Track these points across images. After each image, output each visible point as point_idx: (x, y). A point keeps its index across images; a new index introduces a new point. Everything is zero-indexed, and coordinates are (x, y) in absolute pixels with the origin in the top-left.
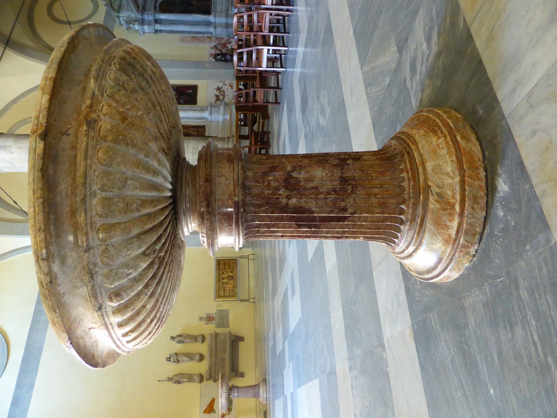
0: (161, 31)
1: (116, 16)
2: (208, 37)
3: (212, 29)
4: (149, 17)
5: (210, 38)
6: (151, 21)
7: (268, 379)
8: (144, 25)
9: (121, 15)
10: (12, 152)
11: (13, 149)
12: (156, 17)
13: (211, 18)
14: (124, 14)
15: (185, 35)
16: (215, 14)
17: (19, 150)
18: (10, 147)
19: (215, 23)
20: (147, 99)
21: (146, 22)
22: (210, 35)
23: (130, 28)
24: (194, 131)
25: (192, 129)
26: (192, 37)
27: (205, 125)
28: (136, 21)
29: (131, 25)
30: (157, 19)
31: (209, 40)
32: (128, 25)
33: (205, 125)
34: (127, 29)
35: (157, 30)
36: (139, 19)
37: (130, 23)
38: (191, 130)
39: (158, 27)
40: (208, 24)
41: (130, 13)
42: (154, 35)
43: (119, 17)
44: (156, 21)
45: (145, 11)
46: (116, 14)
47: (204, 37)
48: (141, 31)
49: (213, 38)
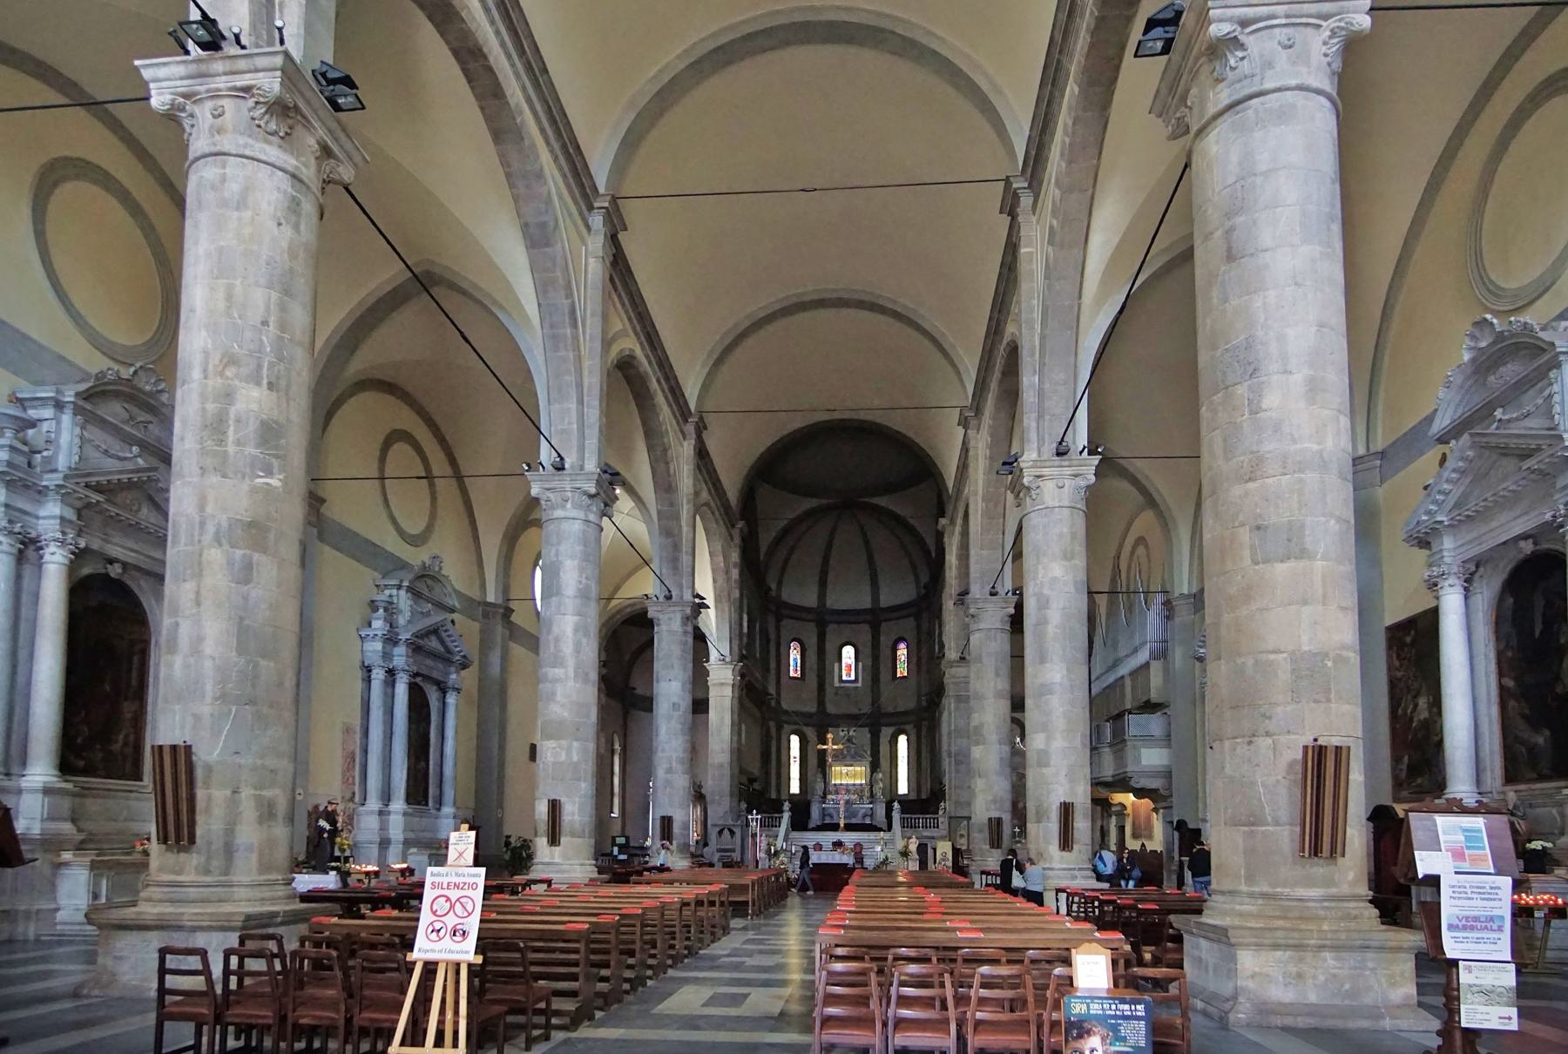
0: (368, 680)
1: (401, 581)
2: (354, 794)
3: (373, 804)
4: (400, 656)
5: (352, 799)
6: (391, 660)
7: (1308, 1014)
8: (384, 642)
9: (402, 593)
10: (280, 224)
11: (287, 231)
12: (52, 548)
13: (398, 805)
14: (403, 600)
15: (358, 736)
16: (411, 815)
17: (285, 244)
18: (296, 227)
19: (389, 813)
20: (1211, 972)
21: (388, 648)
22: (357, 799)
23: (375, 610)
24: (126, 744)
25: (132, 738)
26: (353, 753)
27: (141, 780)
28: (391, 626)
29: (381, 611)
30: (41, 548)
31: (348, 795)
32: (383, 604)
33: (141, 780)
34: (373, 601)
35: (370, 671)
36: (398, 634)
37: (386, 610)
38: (127, 736)
39: (378, 675)
40: (386, 798)
41: (408, 615)
42: (358, 664)
43: (399, 587)
44: (391, 673)
45: (414, 650)
46: (406, 584)
47: (354, 784)
48: (371, 634)
49: (351, 805)
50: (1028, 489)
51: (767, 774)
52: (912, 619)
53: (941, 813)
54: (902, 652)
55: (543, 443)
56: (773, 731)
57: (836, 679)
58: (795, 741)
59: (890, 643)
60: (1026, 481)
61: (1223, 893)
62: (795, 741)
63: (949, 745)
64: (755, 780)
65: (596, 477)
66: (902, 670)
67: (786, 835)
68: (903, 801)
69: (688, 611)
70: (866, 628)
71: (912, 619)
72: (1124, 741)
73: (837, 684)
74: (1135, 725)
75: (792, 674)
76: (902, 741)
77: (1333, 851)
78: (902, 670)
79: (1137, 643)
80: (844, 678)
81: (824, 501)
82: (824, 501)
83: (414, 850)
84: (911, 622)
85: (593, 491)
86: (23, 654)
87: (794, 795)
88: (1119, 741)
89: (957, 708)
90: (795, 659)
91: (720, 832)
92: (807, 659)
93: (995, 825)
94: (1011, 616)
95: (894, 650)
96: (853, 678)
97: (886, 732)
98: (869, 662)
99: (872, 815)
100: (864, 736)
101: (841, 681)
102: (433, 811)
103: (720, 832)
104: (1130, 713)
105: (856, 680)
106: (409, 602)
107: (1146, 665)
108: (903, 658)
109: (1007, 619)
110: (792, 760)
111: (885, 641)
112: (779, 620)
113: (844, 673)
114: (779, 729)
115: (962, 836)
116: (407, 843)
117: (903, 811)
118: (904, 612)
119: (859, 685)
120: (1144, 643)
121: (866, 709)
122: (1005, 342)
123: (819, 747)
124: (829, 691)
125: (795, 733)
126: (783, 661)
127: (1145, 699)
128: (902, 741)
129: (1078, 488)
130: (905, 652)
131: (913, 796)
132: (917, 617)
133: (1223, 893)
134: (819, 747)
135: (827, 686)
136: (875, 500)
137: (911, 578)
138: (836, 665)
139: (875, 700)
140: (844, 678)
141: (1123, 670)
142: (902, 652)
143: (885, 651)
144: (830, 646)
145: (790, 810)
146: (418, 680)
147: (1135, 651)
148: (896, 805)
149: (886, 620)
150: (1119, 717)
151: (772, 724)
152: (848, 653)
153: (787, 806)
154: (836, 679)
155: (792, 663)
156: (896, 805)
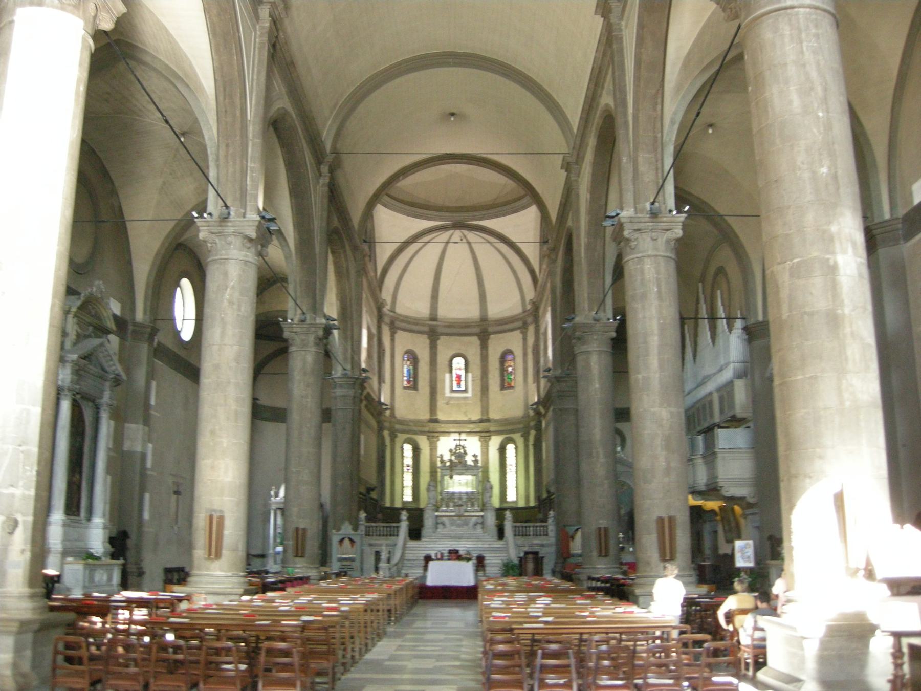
50: (628, 240)
55: (211, 190)
60: (626, 233)
64: (373, 490)
65: (257, 223)
67: (405, 544)
68: (515, 510)
69: (321, 333)
70: (475, 340)
72: (715, 453)
73: (448, 393)
74: (724, 437)
79: (722, 362)
80: (455, 387)
83: (70, 559)
84: (517, 335)
85: (253, 235)
86: (49, 432)
87: (407, 502)
88: (710, 455)
91: (341, 541)
93: (603, 535)
94: (613, 339)
96: (463, 388)
98: (478, 373)
102: (84, 521)
103: (341, 541)
104: (720, 427)
106: (76, 327)
107: (730, 384)
109: (609, 341)
110: (405, 469)
112: (394, 329)
114: (393, 437)
116: (65, 553)
117: (515, 520)
119: (469, 394)
120: (727, 364)
122: (600, 108)
127: (731, 414)
129: (668, 241)
131: (522, 504)
141: (710, 387)
144: (442, 359)
145: (409, 519)
146: (78, 396)
147: (721, 370)
148: (508, 514)
150: (709, 431)
151: (386, 433)
153: (404, 515)
156: (508, 514)
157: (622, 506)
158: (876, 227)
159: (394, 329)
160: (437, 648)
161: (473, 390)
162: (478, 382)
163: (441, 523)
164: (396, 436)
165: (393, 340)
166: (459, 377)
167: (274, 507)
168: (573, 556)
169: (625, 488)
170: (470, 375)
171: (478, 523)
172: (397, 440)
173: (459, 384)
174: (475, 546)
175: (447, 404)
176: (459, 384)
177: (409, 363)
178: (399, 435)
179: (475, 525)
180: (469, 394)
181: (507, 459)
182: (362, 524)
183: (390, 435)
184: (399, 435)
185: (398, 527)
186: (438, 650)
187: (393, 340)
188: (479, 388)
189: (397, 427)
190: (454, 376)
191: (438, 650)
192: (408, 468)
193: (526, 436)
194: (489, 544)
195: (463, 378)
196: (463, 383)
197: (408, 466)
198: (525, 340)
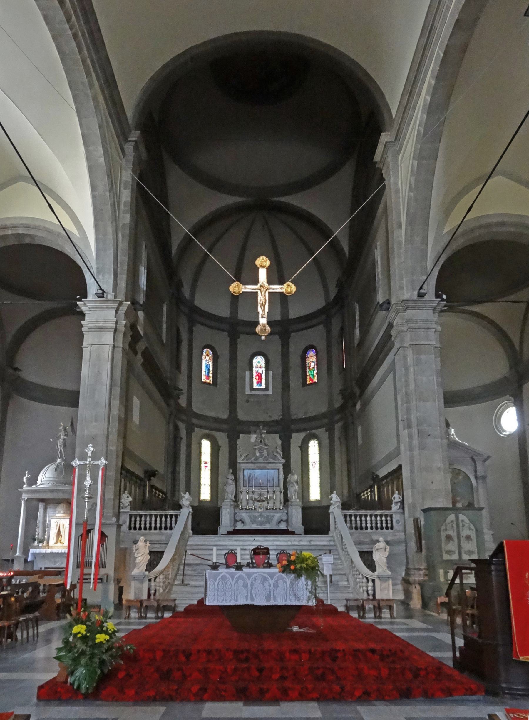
51: (174, 473)
52: (321, 327)
53: (395, 507)
54: (312, 360)
56: (183, 433)
57: (247, 388)
58: (206, 446)
59: (300, 353)
61: (189, 575)
62: (206, 446)
63: (408, 411)
66: (312, 376)
71: (321, 327)
73: (248, 391)
75: (204, 379)
76: (314, 446)
77: (107, 581)
78: (312, 376)
81: (239, 200)
82: (239, 200)
87: (205, 502)
89: (418, 362)
90: (207, 366)
92: (219, 366)
95: (304, 358)
96: (263, 386)
97: (297, 438)
99: (287, 521)
100: (276, 440)
101: (252, 389)
105: (267, 389)
108: (312, 365)
110: (203, 465)
111: (295, 349)
112: (192, 323)
113: (255, 382)
115: (449, 538)
118: (314, 322)
119: (270, 392)
121: (276, 416)
123: (236, 288)
124: (240, 399)
125: (208, 437)
126: (195, 365)
128: (314, 446)
130: (315, 359)
132: (327, 324)
133: (189, 575)
134: (236, 288)
135: (239, 395)
136: (283, 199)
137: (319, 287)
138: (247, 373)
139: (286, 408)
140: (255, 386)
142: (312, 360)
143: (294, 360)
144: (242, 356)
149: (294, 331)
151: (182, 426)
152: (259, 362)
154: (247, 388)
155: (204, 368)
157: (458, 499)
158: (181, 605)
159: (192, 323)
160: (404, 195)
161: (273, 387)
162: (279, 379)
163: (241, 520)
164: (193, 431)
165: (191, 331)
166: (260, 376)
167: (25, 497)
168: (45, 509)
169: (461, 477)
170: (271, 373)
171: (282, 520)
172: (193, 434)
173: (259, 383)
174: (289, 543)
175: (248, 401)
176: (259, 383)
177: (207, 358)
178: (196, 429)
179: (280, 522)
180: (270, 392)
181: (310, 456)
182: (125, 512)
183: (187, 429)
184: (196, 429)
185: (176, 516)
186: (402, 196)
187: (191, 331)
188: (279, 387)
189: (194, 421)
190: (255, 374)
191: (402, 196)
192: (206, 465)
193: (330, 430)
194: (310, 541)
195: (263, 376)
196: (263, 382)
197: (206, 463)
198: (328, 332)
